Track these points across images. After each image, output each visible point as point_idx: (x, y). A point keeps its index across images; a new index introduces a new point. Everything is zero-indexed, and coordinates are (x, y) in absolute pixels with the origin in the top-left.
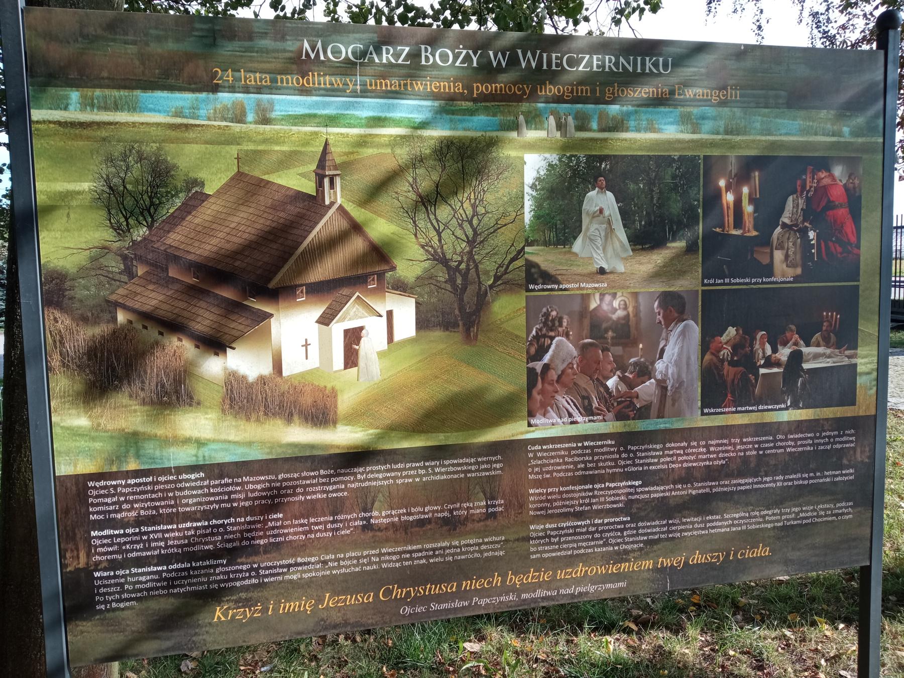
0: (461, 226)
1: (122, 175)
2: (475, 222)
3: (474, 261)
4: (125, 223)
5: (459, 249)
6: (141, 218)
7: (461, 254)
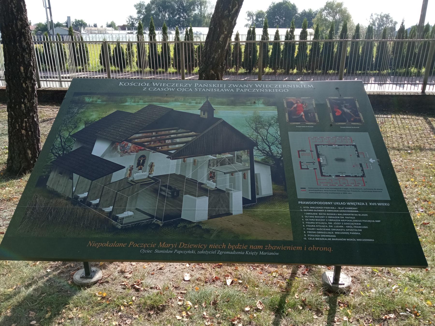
4: (268, 149)
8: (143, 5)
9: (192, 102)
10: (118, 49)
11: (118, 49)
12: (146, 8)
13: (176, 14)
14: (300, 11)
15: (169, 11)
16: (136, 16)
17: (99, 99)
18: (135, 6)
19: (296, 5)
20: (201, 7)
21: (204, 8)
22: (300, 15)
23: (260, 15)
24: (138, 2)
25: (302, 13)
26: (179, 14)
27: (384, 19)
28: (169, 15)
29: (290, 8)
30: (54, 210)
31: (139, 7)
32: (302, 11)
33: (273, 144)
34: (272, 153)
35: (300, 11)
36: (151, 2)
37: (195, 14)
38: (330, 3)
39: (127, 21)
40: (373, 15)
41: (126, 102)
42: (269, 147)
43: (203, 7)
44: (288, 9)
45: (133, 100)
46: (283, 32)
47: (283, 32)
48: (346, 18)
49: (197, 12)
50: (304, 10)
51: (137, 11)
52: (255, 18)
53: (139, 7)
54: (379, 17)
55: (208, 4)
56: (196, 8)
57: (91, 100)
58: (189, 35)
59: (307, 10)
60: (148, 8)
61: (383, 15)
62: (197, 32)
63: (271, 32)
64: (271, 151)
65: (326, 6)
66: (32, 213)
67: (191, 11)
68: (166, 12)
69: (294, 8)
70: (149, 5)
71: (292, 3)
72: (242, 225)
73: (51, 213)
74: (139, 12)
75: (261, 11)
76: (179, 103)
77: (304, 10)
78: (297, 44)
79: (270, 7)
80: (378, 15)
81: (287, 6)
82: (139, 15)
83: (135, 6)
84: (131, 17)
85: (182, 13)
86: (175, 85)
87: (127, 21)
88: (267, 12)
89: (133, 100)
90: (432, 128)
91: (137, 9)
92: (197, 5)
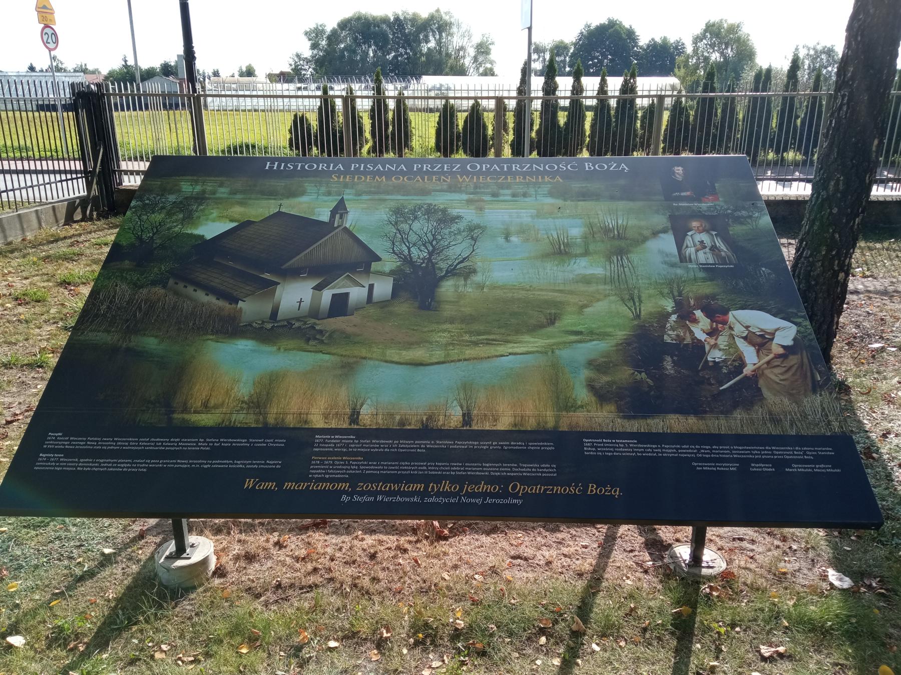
0: (424, 245)
1: (410, 222)
2: (434, 243)
3: (432, 263)
4: (407, 251)
5: (422, 256)
6: (423, 248)
7: (424, 259)
8: (323, 32)
9: (502, 191)
10: (475, 113)
11: (475, 113)
12: (329, 38)
13: (391, 49)
14: (643, 40)
15: (376, 45)
16: (307, 53)
17: (221, 185)
18: (306, 33)
19: (636, 30)
20: (441, 35)
21: (447, 35)
22: (644, 50)
23: (559, 49)
24: (313, 26)
25: (648, 46)
26: (396, 50)
27: (823, 56)
28: (375, 52)
29: (624, 36)
30: (145, 304)
31: (315, 35)
32: (647, 42)
33: (414, 245)
34: (411, 258)
35: (643, 40)
36: (339, 25)
37: (429, 49)
38: (713, 25)
39: (291, 65)
40: (800, 48)
41: (303, 193)
42: (409, 248)
43: (444, 34)
44: (621, 38)
45: (323, 189)
46: (615, 84)
47: (615, 84)
48: (746, 54)
49: (432, 44)
50: (653, 39)
51: (309, 44)
52: (548, 57)
53: (315, 35)
54: (812, 52)
55: (454, 29)
56: (431, 38)
57: (198, 188)
58: (628, 89)
59: (658, 40)
60: (333, 37)
61: (819, 48)
62: (441, 85)
63: (591, 84)
64: (410, 255)
65: (706, 31)
66: (108, 307)
67: (420, 43)
68: (370, 46)
69: (631, 35)
70: (334, 32)
71: (627, 26)
72: (355, 326)
73: (140, 308)
74: (314, 46)
75: (562, 42)
76: (465, 197)
77: (653, 39)
78: (589, 108)
79: (581, 33)
80: (809, 50)
81: (616, 31)
82: (315, 52)
83: (306, 33)
84: (298, 56)
85: (403, 47)
86: (442, 167)
87: (291, 65)
88: (575, 44)
89: (323, 189)
90: (4, 231)
91: (310, 40)
92: (433, 31)
